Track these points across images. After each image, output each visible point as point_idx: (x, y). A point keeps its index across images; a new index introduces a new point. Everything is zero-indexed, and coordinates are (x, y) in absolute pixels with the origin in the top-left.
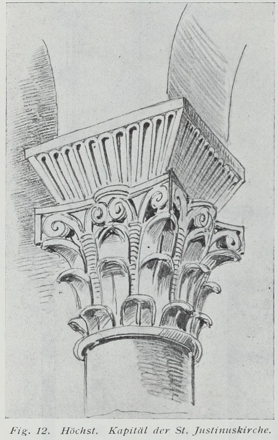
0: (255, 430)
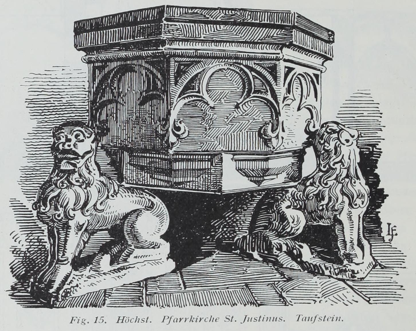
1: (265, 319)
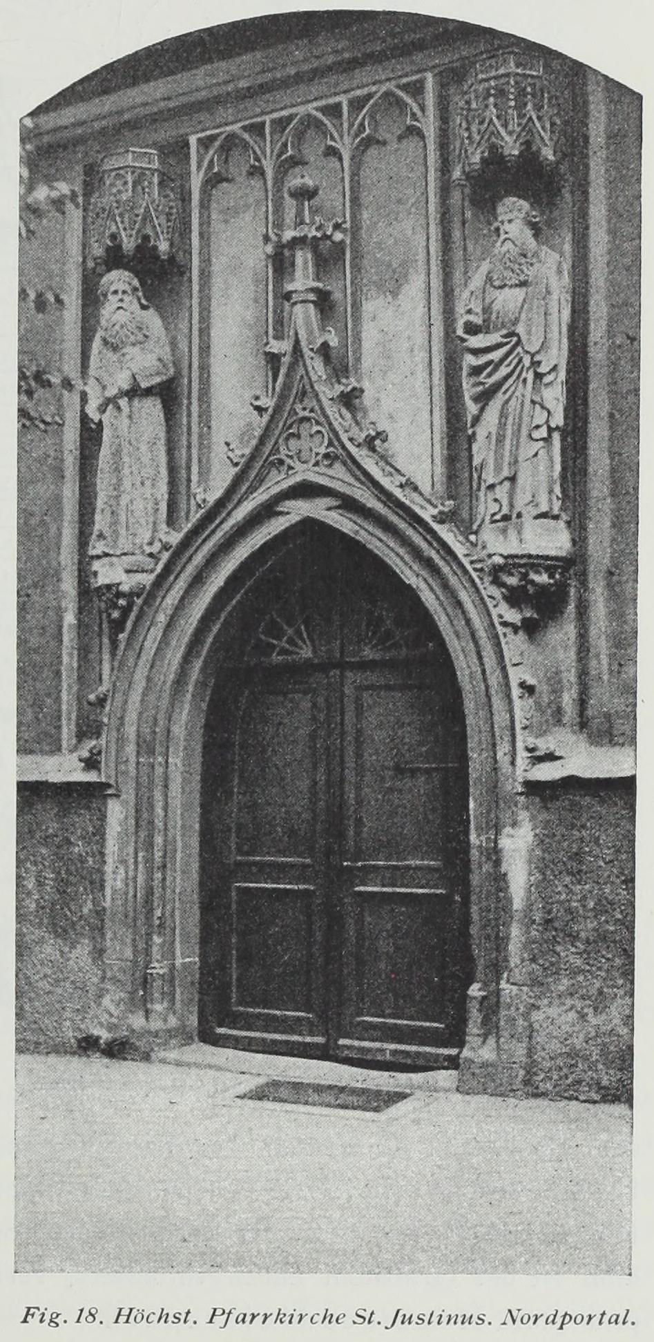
1: (445, 1319)
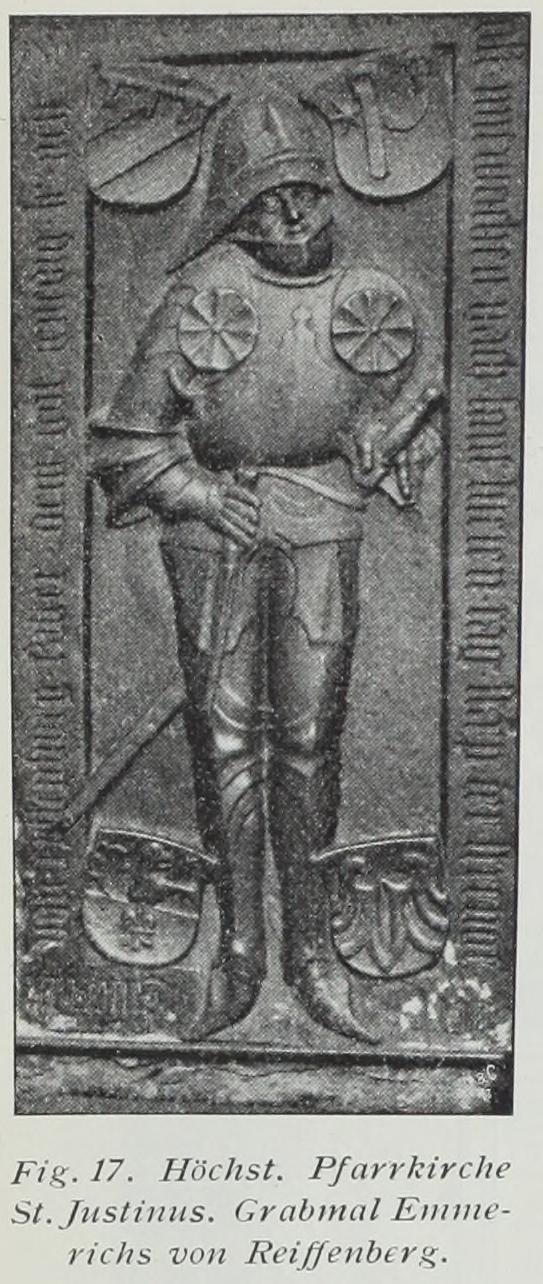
0: (217, 1169)
1: (145, 1215)
